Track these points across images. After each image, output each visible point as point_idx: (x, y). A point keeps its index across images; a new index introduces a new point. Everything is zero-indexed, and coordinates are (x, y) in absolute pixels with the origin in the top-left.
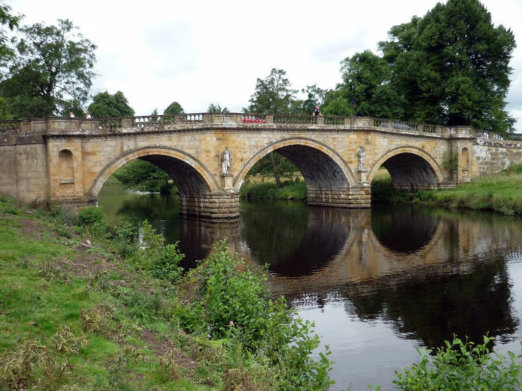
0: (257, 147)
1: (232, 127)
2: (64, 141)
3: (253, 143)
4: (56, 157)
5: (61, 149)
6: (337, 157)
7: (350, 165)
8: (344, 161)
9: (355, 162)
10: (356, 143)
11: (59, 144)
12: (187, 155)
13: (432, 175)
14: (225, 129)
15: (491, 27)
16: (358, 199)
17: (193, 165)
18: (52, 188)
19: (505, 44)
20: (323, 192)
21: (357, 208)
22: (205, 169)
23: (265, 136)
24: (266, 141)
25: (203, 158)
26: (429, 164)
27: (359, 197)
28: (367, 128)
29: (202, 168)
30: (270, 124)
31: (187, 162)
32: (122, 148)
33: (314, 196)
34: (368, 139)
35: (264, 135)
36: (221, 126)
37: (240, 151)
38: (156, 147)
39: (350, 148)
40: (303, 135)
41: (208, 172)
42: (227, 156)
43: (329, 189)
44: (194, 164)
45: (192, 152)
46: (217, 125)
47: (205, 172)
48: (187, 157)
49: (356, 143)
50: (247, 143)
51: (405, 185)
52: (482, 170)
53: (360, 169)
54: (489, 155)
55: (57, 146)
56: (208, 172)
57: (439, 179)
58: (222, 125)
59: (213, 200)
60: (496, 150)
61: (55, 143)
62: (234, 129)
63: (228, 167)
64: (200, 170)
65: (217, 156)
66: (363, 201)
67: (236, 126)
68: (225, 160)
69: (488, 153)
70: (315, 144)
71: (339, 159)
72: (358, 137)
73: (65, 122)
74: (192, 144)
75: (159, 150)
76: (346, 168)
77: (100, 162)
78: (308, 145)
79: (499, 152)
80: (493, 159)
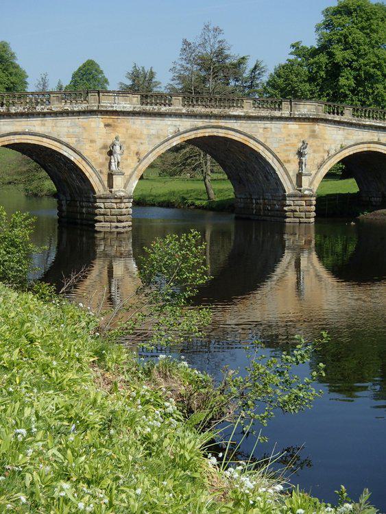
0: (158, 137)
1: (125, 110)
3: (153, 132)
7: (286, 165)
9: (294, 162)
10: (296, 136)
16: (296, 211)
20: (254, 201)
23: (169, 123)
27: (297, 208)
28: (314, 115)
31: (65, 154)
34: (314, 131)
36: (110, 109)
39: (288, 142)
40: (222, 123)
42: (117, 148)
43: (261, 197)
44: (73, 157)
45: (72, 142)
46: (106, 107)
49: (296, 136)
50: (145, 132)
51: (375, 195)
63: (118, 163)
64: (82, 165)
65: (105, 147)
67: (131, 109)
74: (71, 130)
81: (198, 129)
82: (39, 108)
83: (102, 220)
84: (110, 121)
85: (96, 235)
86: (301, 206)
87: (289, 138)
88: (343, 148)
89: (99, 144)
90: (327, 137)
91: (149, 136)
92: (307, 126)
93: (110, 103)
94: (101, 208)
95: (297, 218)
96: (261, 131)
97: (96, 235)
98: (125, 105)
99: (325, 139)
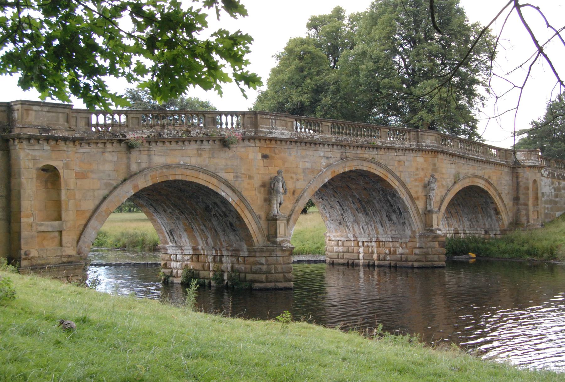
1: (283, 137)
2: (36, 148)
3: (308, 165)
4: (32, 179)
5: (41, 165)
6: (403, 191)
7: (417, 202)
8: (411, 197)
10: (423, 169)
11: (37, 153)
12: (223, 183)
13: (494, 218)
14: (276, 140)
15: (280, 64)
17: (230, 200)
18: (23, 242)
19: (198, 100)
21: (267, 290)
22: (247, 206)
24: (324, 162)
25: (244, 186)
26: (493, 202)
28: (435, 147)
29: (242, 205)
30: (327, 136)
32: (128, 167)
33: (341, 249)
35: (322, 152)
36: (269, 135)
37: (292, 178)
38: (179, 166)
39: (417, 177)
40: (366, 154)
41: (251, 211)
43: (374, 239)
44: (231, 198)
45: (229, 177)
46: (265, 133)
47: (246, 212)
48: (223, 187)
50: (301, 165)
52: (546, 211)
53: (429, 208)
54: (553, 190)
55: (34, 158)
56: (251, 211)
57: (505, 223)
58: (271, 133)
59: (257, 259)
60: (559, 183)
61: (31, 152)
62: (286, 141)
65: (263, 185)
66: (436, 257)
67: (288, 137)
68: (277, 192)
69: (551, 187)
70: (379, 169)
71: (405, 193)
72: (425, 161)
73: (48, 112)
74: (229, 163)
75: (185, 171)
76: (413, 207)
77: (94, 190)
78: (372, 171)
79: (562, 186)
80: (557, 196)
81: (501, 197)
82: (436, 15)
83: (264, 280)
84: (267, 152)
85: (183, 93)
86: (434, 248)
87: (417, 172)
88: (499, 195)
89: (257, 182)
90: (444, 171)
91: (304, 170)
92: (430, 158)
93: (268, 128)
94: (262, 264)
95: (430, 261)
96: (396, 164)
97: (183, 93)
98: (283, 131)
99: (443, 174)
